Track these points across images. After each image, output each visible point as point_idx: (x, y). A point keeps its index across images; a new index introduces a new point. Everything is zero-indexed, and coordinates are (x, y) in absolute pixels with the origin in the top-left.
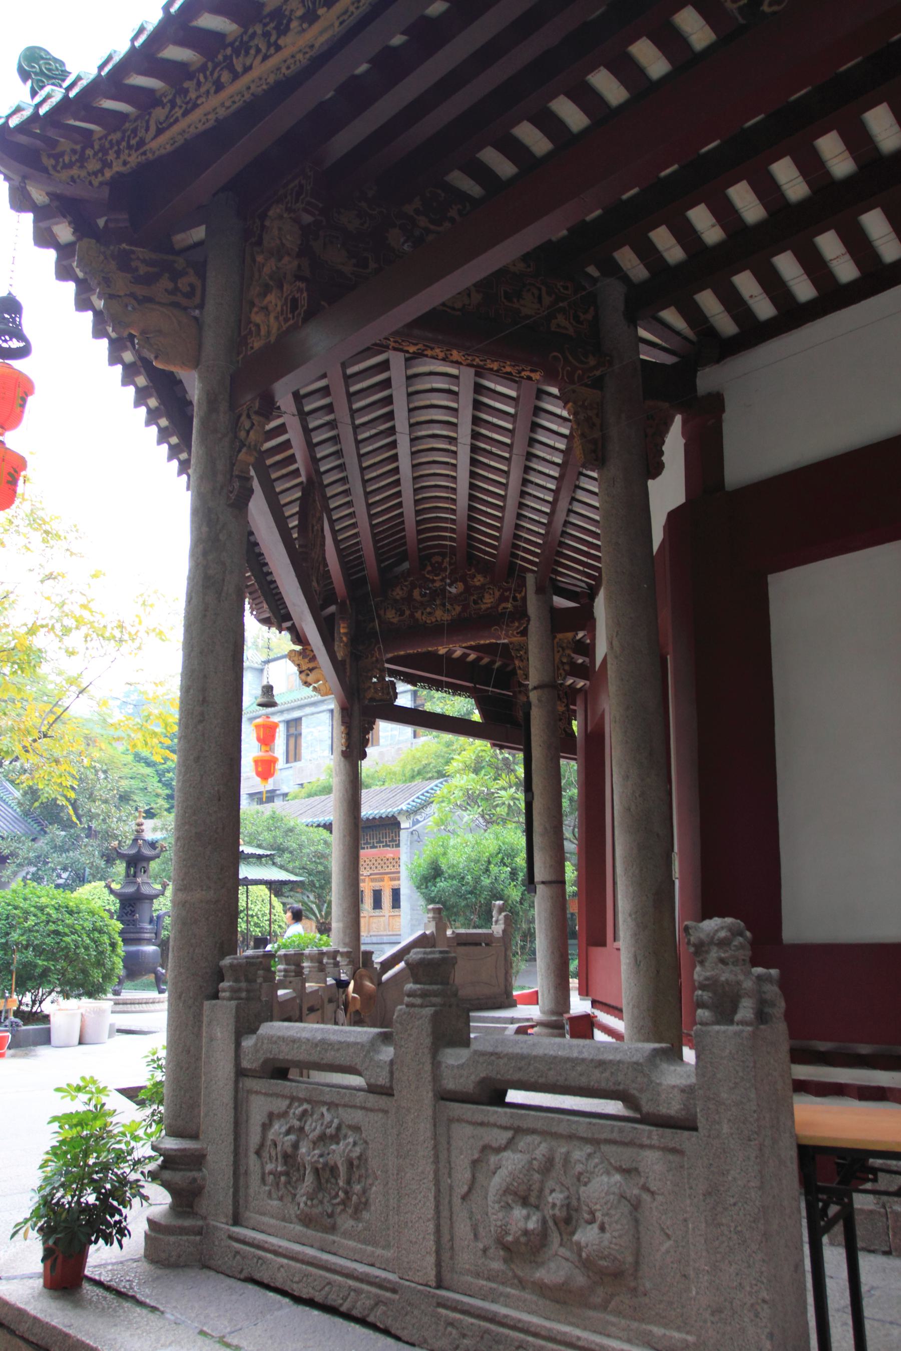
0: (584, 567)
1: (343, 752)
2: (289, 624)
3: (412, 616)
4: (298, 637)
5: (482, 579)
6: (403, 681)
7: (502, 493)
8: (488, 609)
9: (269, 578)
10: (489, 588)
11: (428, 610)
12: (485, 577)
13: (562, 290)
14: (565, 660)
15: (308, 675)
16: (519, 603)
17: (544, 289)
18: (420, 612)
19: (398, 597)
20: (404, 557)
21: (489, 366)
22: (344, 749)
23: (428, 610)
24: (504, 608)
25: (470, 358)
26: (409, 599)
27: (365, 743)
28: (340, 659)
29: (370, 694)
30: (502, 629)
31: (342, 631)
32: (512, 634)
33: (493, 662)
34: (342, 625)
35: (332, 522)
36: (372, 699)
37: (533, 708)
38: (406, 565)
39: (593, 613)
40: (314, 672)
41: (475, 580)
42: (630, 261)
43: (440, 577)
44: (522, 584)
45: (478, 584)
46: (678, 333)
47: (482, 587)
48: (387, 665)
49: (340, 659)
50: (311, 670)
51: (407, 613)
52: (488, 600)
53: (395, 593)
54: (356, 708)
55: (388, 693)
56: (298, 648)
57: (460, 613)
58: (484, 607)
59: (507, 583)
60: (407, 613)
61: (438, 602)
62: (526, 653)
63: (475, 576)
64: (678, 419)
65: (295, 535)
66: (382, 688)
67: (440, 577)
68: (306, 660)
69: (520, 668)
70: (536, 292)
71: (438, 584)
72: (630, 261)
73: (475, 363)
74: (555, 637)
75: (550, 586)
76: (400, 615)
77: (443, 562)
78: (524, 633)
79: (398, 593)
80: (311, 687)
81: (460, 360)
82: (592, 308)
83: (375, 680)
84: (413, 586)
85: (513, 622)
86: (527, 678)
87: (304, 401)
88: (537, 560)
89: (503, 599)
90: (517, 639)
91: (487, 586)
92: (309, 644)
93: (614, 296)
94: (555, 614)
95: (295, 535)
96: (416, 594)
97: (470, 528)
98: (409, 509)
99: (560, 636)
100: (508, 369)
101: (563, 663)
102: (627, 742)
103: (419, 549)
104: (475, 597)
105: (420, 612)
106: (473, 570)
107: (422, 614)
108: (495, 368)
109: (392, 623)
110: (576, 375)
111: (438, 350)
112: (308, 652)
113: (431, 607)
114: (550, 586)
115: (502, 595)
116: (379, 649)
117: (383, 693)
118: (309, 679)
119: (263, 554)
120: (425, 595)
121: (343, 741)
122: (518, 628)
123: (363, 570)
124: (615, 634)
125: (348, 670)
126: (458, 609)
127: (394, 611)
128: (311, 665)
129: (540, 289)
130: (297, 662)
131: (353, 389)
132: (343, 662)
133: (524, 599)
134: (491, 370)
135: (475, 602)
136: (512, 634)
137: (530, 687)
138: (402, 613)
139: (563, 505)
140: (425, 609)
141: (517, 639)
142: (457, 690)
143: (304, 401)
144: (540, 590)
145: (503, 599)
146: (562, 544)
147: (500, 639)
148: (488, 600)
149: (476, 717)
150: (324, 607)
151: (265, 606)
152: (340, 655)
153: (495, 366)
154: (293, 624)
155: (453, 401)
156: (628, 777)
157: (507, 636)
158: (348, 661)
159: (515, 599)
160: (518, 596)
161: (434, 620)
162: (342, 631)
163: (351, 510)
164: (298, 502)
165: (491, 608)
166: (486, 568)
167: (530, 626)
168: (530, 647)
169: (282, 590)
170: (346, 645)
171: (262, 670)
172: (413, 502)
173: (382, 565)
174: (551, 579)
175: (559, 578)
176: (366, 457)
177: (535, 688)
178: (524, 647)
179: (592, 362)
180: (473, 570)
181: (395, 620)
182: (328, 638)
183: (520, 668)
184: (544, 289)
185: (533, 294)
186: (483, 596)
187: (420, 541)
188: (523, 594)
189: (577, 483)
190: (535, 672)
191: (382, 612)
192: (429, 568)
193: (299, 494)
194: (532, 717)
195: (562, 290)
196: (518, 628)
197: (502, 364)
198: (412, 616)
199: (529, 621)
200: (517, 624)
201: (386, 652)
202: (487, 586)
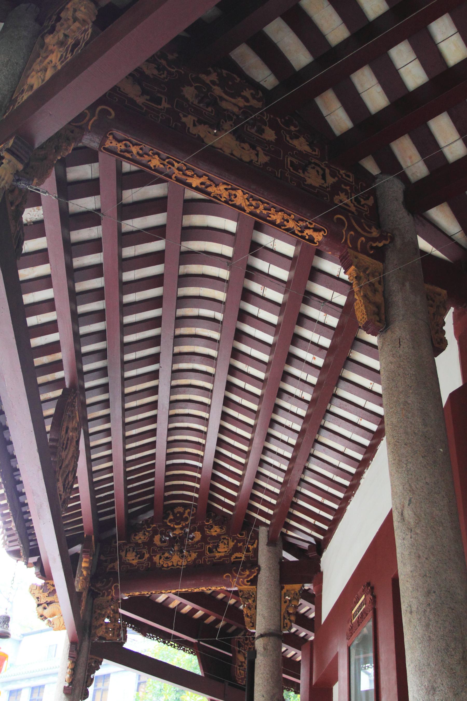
0: (316, 519)
1: (65, 688)
2: (35, 559)
3: (150, 559)
4: (44, 573)
5: (218, 530)
6: (133, 628)
7: (240, 472)
8: (221, 557)
9: (24, 509)
10: (224, 539)
11: (166, 555)
12: (221, 528)
13: (344, 176)
14: (291, 611)
15: (45, 608)
16: (250, 554)
17: (327, 171)
18: (158, 556)
19: (140, 541)
20: (151, 505)
21: (273, 217)
22: (67, 685)
23: (166, 555)
24: (236, 558)
25: (254, 203)
26: (150, 543)
27: (89, 681)
28: (77, 590)
29: (101, 632)
30: (234, 577)
31: (84, 565)
32: (243, 582)
33: (217, 621)
34: (84, 560)
35: (89, 449)
36: (101, 638)
37: (258, 655)
38: (150, 514)
39: (320, 567)
40: (51, 606)
41: (212, 530)
42: (410, 158)
43: (180, 526)
44: (256, 537)
45: (214, 534)
46: (450, 238)
47: (218, 537)
48: (121, 611)
49: (77, 590)
50: (49, 604)
51: (147, 556)
52: (223, 549)
53: (137, 538)
54: (86, 644)
55: (119, 635)
56: (41, 582)
57: (195, 559)
58: (218, 555)
59: (242, 535)
60: (147, 556)
61: (176, 548)
62: (255, 601)
63: (212, 527)
64: (452, 309)
65: (48, 428)
66: (113, 629)
67: (180, 526)
68: (46, 594)
69: (248, 616)
70: (321, 172)
71: (177, 532)
72: (410, 158)
73: (258, 211)
74: (282, 588)
75: (280, 540)
76: (139, 558)
77: (184, 513)
78: (254, 582)
79: (141, 538)
80: (46, 621)
81: (243, 205)
82: (372, 197)
83: (107, 620)
84: (155, 532)
85: (243, 570)
86: (254, 626)
87: (85, 376)
88: (271, 512)
89: (236, 549)
90: (247, 587)
91: (223, 537)
92: (51, 579)
93: (393, 190)
94: (283, 563)
95: (48, 428)
96: (157, 539)
97: (215, 477)
98: (161, 451)
99: (287, 587)
100: (291, 224)
101: (289, 614)
102: (430, 639)
103: (165, 497)
104: (210, 546)
105: (158, 556)
106: (211, 522)
107: (160, 558)
108: (278, 222)
109: (131, 565)
110: (359, 242)
111: (222, 187)
112: (49, 586)
113: (169, 553)
114: (280, 540)
115: (235, 545)
116: (116, 587)
117: (113, 634)
118: (46, 613)
119: (18, 470)
120: (164, 542)
121: (68, 676)
122: (248, 576)
123: (113, 512)
124: (407, 503)
125: (83, 603)
126: (194, 555)
127: (134, 554)
128: (49, 599)
129: (324, 170)
130: (37, 595)
131: (128, 405)
132: (80, 594)
133: (256, 551)
134: (273, 223)
135: (210, 551)
136: (243, 582)
137: (256, 635)
138: (142, 557)
139: (300, 461)
140: (163, 554)
141: (247, 587)
142: (182, 644)
143: (92, 451)
144: (271, 542)
145: (236, 549)
146: (298, 494)
147: (230, 586)
148: (223, 549)
149: (198, 671)
150: (71, 545)
151: (13, 524)
152: (78, 586)
153: (278, 218)
154: (40, 559)
155: (209, 382)
156: (434, 689)
157: (238, 584)
158: (85, 594)
159: (248, 550)
160: (251, 547)
161: (170, 564)
162: (84, 565)
163: (106, 426)
164: (57, 400)
165: (225, 556)
166: (222, 520)
167: (259, 576)
168: (259, 596)
169: (36, 531)
170: (85, 579)
171: (20, 641)
172: (168, 403)
173: (130, 511)
174: (282, 533)
175: (290, 533)
176: (129, 439)
177: (261, 636)
178: (252, 596)
179: (375, 233)
180: (211, 522)
181: (135, 562)
182: (70, 565)
183: (248, 616)
184: (327, 171)
185: (318, 172)
186: (218, 546)
187: (168, 478)
188: (255, 546)
189: (312, 452)
190: (262, 622)
191: (123, 554)
192: (171, 517)
193: (59, 392)
194: (257, 666)
195: (344, 176)
196: (248, 576)
197: (286, 217)
198: (150, 559)
199: (259, 570)
200: (247, 573)
201: (123, 591)
202: (223, 537)
